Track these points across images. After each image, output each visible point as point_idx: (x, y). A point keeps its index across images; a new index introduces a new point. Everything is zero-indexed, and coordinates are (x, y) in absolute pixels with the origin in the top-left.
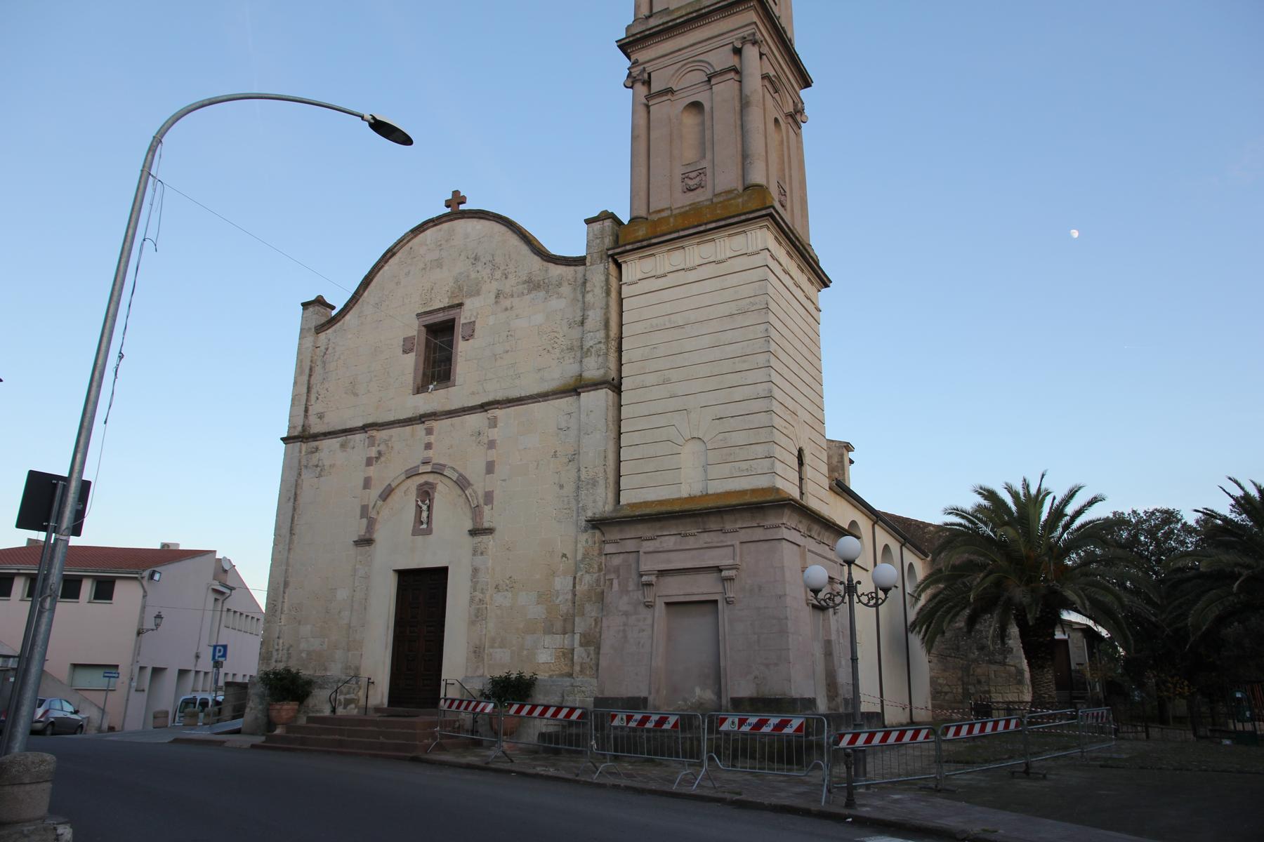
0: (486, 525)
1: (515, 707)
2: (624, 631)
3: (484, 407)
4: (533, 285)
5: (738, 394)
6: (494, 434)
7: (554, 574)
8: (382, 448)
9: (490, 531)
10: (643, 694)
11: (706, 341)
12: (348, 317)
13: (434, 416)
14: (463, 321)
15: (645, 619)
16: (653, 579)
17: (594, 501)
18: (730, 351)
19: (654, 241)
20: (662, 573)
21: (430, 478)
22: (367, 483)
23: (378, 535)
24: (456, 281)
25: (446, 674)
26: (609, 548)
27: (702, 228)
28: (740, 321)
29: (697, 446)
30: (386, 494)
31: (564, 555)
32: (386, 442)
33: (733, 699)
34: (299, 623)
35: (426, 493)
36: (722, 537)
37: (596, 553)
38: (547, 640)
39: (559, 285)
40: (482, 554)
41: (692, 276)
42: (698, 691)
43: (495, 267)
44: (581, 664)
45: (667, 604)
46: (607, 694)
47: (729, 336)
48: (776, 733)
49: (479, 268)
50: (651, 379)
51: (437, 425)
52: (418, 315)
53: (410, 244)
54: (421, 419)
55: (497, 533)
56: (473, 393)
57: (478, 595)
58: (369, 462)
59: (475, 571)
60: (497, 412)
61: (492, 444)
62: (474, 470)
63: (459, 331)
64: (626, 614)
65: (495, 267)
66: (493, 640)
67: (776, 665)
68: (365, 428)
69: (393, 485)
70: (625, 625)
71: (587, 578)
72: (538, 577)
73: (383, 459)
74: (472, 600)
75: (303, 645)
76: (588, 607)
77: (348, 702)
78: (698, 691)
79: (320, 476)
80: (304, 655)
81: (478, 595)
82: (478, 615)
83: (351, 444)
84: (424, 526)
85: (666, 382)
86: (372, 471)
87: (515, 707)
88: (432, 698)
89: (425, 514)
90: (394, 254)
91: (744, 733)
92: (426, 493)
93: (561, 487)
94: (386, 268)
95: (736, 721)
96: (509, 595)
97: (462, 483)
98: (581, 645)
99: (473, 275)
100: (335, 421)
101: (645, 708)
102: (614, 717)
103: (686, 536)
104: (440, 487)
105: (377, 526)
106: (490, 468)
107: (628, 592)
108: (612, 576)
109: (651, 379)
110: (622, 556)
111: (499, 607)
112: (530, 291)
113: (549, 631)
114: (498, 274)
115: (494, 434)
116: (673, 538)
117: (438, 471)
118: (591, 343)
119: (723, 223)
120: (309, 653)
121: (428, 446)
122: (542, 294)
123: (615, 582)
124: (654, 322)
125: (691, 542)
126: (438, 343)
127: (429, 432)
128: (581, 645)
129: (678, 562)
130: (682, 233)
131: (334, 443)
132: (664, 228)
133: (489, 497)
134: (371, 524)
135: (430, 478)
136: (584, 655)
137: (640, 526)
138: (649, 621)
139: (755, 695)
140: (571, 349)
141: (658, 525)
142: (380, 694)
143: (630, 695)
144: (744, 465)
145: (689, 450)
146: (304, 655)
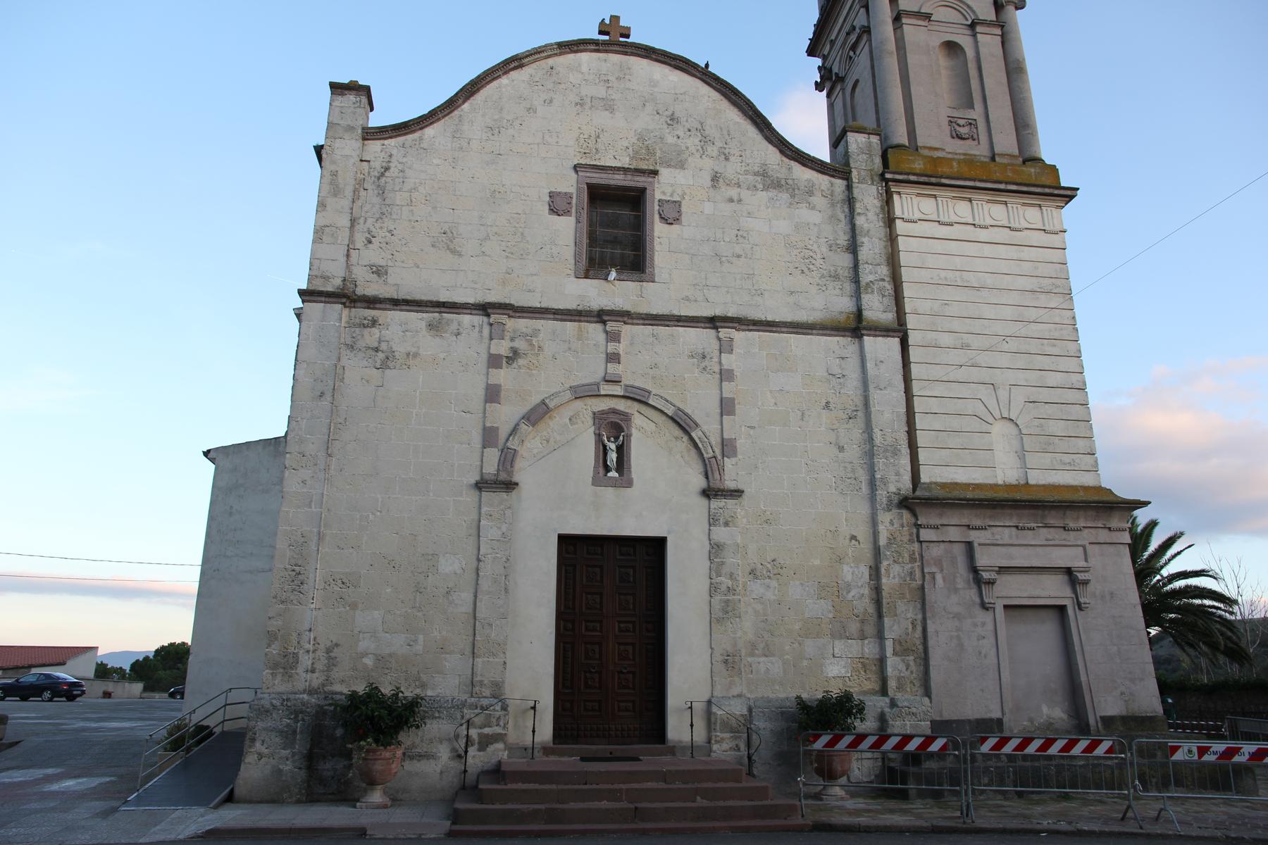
0: (730, 484)
1: (825, 739)
2: (958, 637)
3: (713, 322)
4: (773, 184)
5: (1054, 379)
6: (728, 361)
7: (840, 560)
8: (520, 344)
9: (737, 493)
10: (996, 714)
11: (1008, 312)
12: (429, 132)
13: (625, 316)
14: (658, 196)
15: (984, 624)
16: (993, 576)
17: (897, 474)
18: (1035, 329)
19: (944, 181)
20: (1002, 570)
21: (622, 405)
22: (492, 394)
23: (524, 474)
24: (641, 138)
25: (675, 699)
26: (925, 534)
27: (1002, 186)
28: (1043, 300)
29: (1009, 428)
30: (538, 414)
31: (853, 538)
32: (529, 337)
33: (1102, 718)
34: (354, 606)
35: (613, 430)
36: (1064, 534)
37: (906, 539)
38: (839, 646)
39: (810, 193)
40: (726, 524)
41: (983, 235)
42: (1045, 709)
43: (705, 140)
44: (899, 679)
45: (1006, 607)
46: (947, 716)
47: (1032, 314)
48: (1222, 761)
49: (681, 134)
50: (946, 339)
51: (627, 330)
52: (576, 168)
53: (551, 61)
54: (601, 316)
55: (745, 496)
56: (687, 299)
57: (725, 581)
58: (494, 361)
59: (716, 549)
60: (739, 336)
61: (725, 375)
62: (700, 402)
63: (653, 210)
64: (957, 616)
65: (705, 140)
66: (753, 646)
67: (1142, 679)
68: (484, 309)
69: (551, 405)
70: (958, 630)
71: (896, 569)
72: (817, 562)
73: (521, 362)
74: (713, 589)
75: (365, 644)
76: (901, 606)
77: (485, 742)
78: (1045, 709)
79: (384, 366)
80: (369, 661)
81: (725, 581)
82: (723, 609)
83: (454, 327)
84: (613, 474)
85: (965, 347)
86: (502, 376)
87: (825, 739)
88: (656, 729)
89: (613, 456)
90: (521, 66)
91: (1208, 763)
92: (613, 430)
93: (841, 449)
94: (504, 80)
95: (1195, 750)
96: (774, 583)
97: (682, 424)
98: (895, 654)
99: (670, 140)
100: (405, 282)
101: (1001, 731)
102: (1174, 749)
103: (1023, 529)
104: (638, 420)
105: (519, 464)
106: (726, 407)
107: (956, 590)
108: (934, 569)
109: (946, 339)
110: (942, 546)
111: (759, 600)
112: (766, 188)
113: (841, 633)
114: (712, 150)
115: (728, 361)
116: (1007, 531)
117: (639, 398)
118: (871, 278)
119: (1025, 189)
120: (379, 659)
121: (613, 358)
122: (785, 196)
123: (939, 577)
124: (943, 274)
125: (1029, 537)
126: (616, 221)
127: (613, 337)
128: (895, 654)
129: (1021, 558)
130: (979, 184)
131: (417, 319)
132: (946, 170)
133: (728, 447)
134: (508, 458)
135: (622, 405)
136: (902, 666)
137: (966, 512)
138: (990, 626)
139: (1124, 713)
140: (835, 277)
141: (989, 512)
142: (546, 732)
143: (978, 716)
144: (1067, 458)
145: (999, 429)
146: (369, 661)
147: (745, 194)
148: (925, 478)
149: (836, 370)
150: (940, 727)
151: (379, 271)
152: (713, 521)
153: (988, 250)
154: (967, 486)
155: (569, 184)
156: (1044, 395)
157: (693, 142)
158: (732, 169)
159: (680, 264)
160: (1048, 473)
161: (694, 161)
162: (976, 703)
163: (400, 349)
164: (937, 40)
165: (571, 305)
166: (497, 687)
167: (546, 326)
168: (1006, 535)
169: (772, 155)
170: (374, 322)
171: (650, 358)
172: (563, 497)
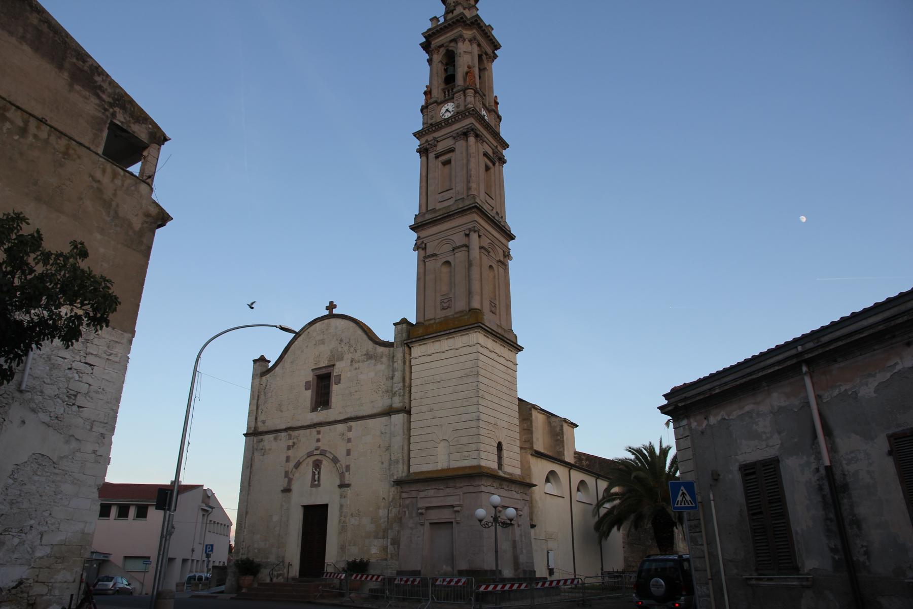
0: (347, 482)
4: (369, 356)
7: (379, 508)
8: (295, 440)
10: (419, 569)
16: (423, 511)
20: (428, 508)
21: (319, 457)
22: (288, 459)
23: (295, 487)
35: (317, 465)
39: (382, 357)
41: (444, 356)
43: (350, 346)
51: (322, 429)
58: (289, 448)
59: (341, 506)
63: (333, 379)
65: (350, 346)
68: (286, 430)
71: (394, 510)
77: (278, 575)
82: (343, 529)
85: (432, 410)
86: (290, 453)
97: (335, 460)
99: (340, 349)
106: (348, 453)
113: (376, 537)
117: (323, 453)
121: (318, 440)
122: (373, 361)
125: (441, 493)
129: (435, 503)
133: (348, 468)
134: (290, 481)
135: (319, 457)
144: (466, 454)
147: (361, 364)
148: (412, 471)
149: (383, 431)
150: (400, 573)
151: (264, 422)
152: (341, 497)
153: (445, 362)
154: (428, 472)
155: (310, 377)
156: (461, 426)
157: (346, 348)
158: (357, 356)
159: (342, 400)
160: (560, 458)
161: (346, 357)
162: (414, 564)
163: (267, 448)
164: (440, 262)
165: (308, 423)
166: (283, 557)
167: (302, 432)
168: (431, 493)
169: (370, 345)
170: (262, 440)
171: (331, 438)
172: (305, 494)
